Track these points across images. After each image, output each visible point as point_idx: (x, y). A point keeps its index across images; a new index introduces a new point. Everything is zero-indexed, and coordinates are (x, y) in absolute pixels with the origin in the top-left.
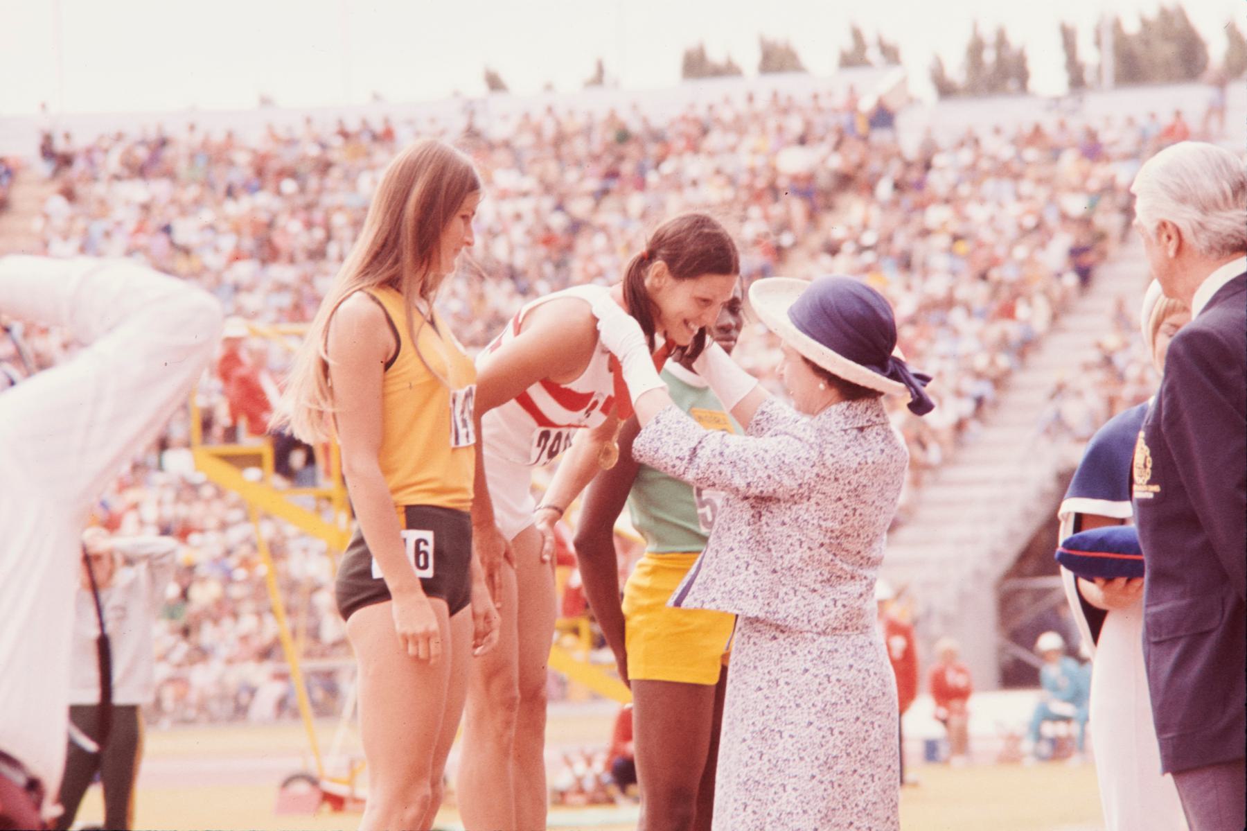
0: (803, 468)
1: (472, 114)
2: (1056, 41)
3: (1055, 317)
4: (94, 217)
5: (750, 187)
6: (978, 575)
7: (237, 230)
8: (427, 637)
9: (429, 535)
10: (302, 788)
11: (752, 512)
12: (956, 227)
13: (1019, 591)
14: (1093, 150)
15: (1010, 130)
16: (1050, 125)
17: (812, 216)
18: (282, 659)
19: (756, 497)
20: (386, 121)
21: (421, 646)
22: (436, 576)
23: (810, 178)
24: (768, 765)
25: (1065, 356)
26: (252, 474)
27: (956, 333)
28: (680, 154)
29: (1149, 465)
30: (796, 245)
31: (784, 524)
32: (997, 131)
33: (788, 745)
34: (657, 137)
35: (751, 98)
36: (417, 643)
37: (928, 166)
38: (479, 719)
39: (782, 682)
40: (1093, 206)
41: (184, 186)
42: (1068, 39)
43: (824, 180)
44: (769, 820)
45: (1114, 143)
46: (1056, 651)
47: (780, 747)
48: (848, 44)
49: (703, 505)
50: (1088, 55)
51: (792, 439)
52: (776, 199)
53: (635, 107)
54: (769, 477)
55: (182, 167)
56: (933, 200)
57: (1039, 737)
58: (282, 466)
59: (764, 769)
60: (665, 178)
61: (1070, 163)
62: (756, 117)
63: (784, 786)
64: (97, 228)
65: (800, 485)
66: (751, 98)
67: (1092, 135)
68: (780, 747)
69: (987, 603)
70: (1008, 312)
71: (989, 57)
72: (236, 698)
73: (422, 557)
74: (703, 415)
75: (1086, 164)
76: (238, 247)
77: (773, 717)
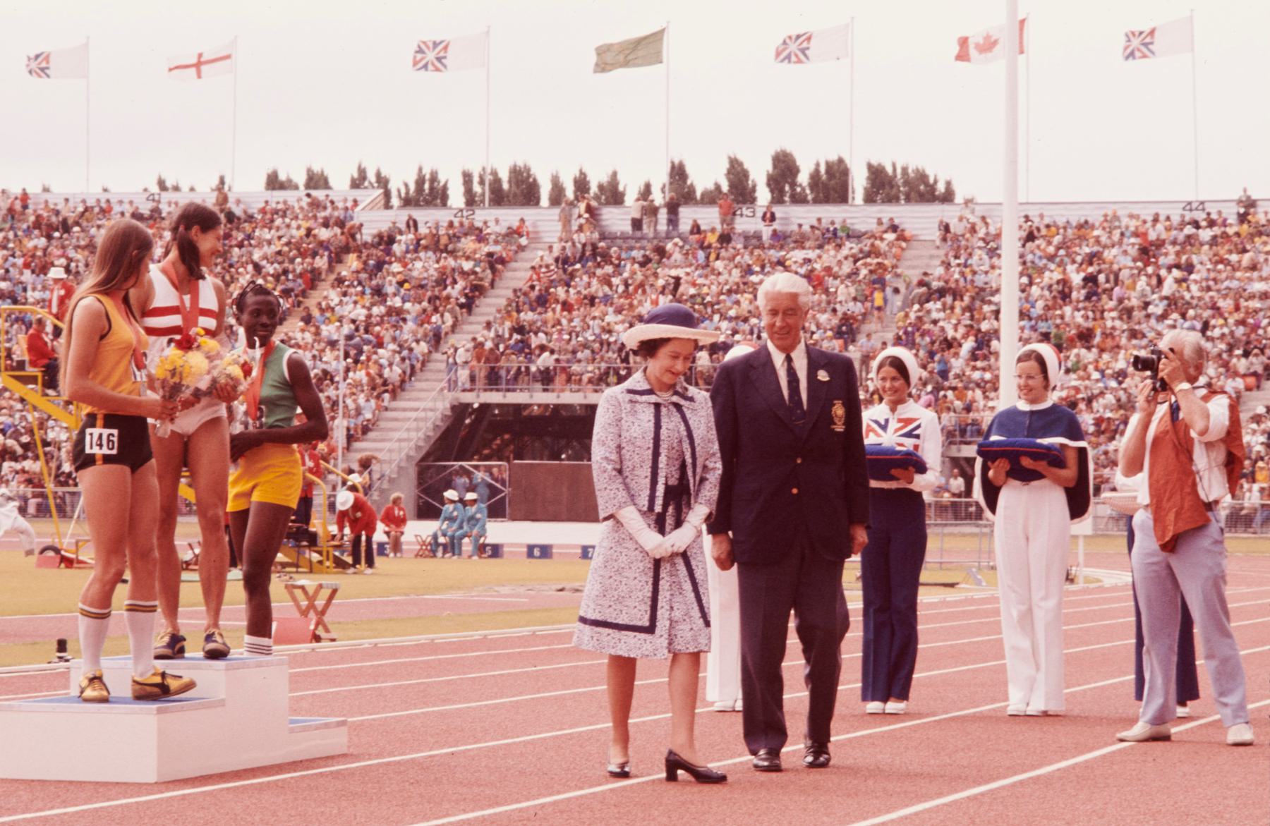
6: (409, 457)
10: (51, 554)
29: (899, 448)
42: (467, 178)
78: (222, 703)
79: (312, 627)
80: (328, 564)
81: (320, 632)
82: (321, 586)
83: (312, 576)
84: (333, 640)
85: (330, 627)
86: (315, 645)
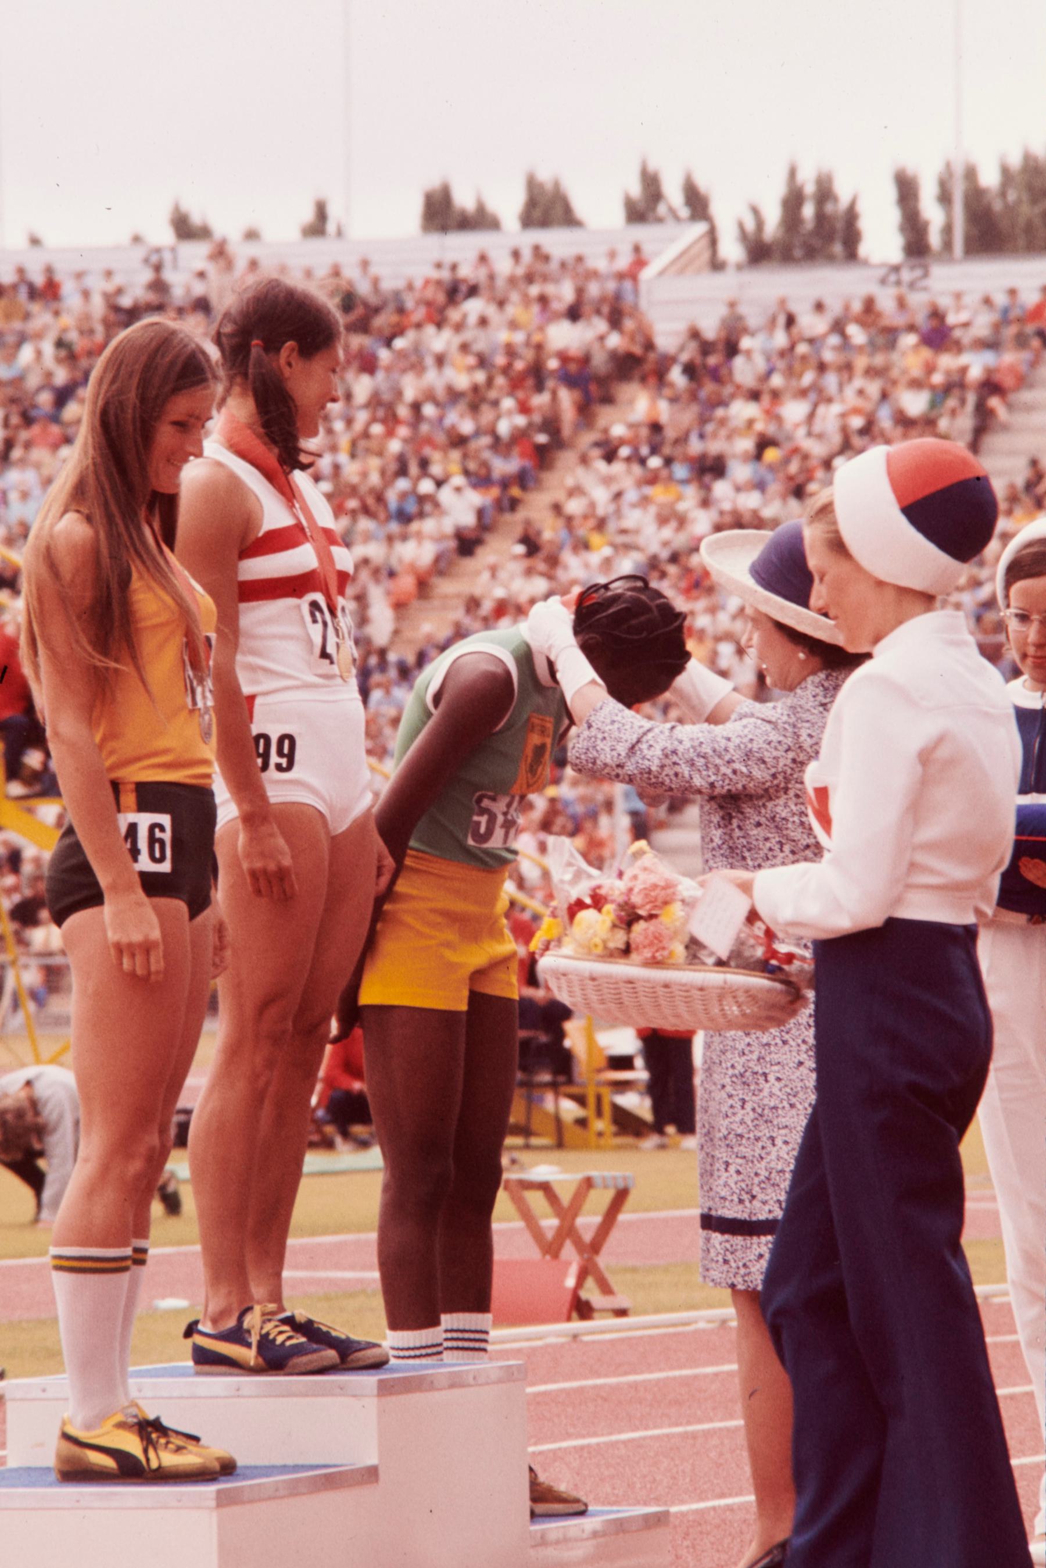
0: (775, 753)
1: (158, 268)
2: (890, 193)
5: (506, 370)
8: (147, 948)
9: (165, 819)
11: (721, 813)
14: (938, 335)
17: (585, 411)
19: (723, 797)
20: (49, 270)
21: (139, 959)
23: (586, 360)
24: (752, 1115)
28: (419, 326)
31: (759, 824)
33: (775, 1091)
36: (133, 956)
37: (732, 349)
38: (233, 1052)
42: (906, 190)
43: (600, 362)
45: (966, 325)
48: (636, 190)
50: (932, 212)
51: (759, 722)
52: (539, 387)
53: (365, 264)
54: (735, 772)
60: (402, 354)
63: (772, 1139)
65: (774, 776)
67: (937, 315)
68: (766, 1093)
71: (808, 211)
75: (926, 353)
77: (755, 1056)
78: (372, 1474)
79: (570, 1282)
80: (599, 1125)
81: (591, 1293)
82: (588, 1183)
83: (557, 1155)
84: (622, 1313)
85: (613, 1280)
86: (577, 1325)
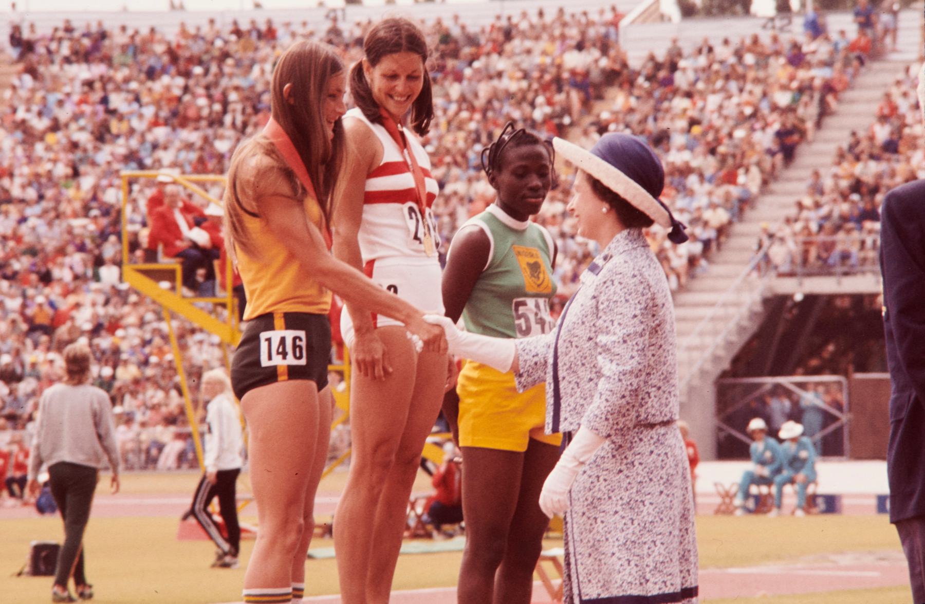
1: (335, 20)
3: (765, 183)
4: (54, 90)
6: (703, 373)
7: (157, 103)
12: (692, 113)
13: (734, 386)
15: (735, 42)
16: (765, 39)
17: (586, 104)
18: (185, 423)
22: (308, 362)
23: (587, 74)
25: (771, 212)
26: (165, 285)
27: (690, 193)
28: (488, 54)
30: (572, 124)
32: (726, 42)
34: (472, 41)
35: (541, 14)
39: (636, 463)
40: (795, 101)
41: (116, 70)
43: (595, 76)
44: (648, 570)
46: (761, 431)
47: (645, 513)
49: (519, 317)
52: (560, 90)
55: (116, 55)
56: (675, 92)
57: (747, 495)
58: (189, 281)
59: (637, 531)
60: (478, 71)
61: (779, 69)
62: (544, 28)
64: (53, 98)
66: (541, 14)
69: (709, 394)
70: (731, 178)
72: (148, 451)
73: (298, 350)
74: (521, 250)
76: (156, 116)
77: (634, 490)
